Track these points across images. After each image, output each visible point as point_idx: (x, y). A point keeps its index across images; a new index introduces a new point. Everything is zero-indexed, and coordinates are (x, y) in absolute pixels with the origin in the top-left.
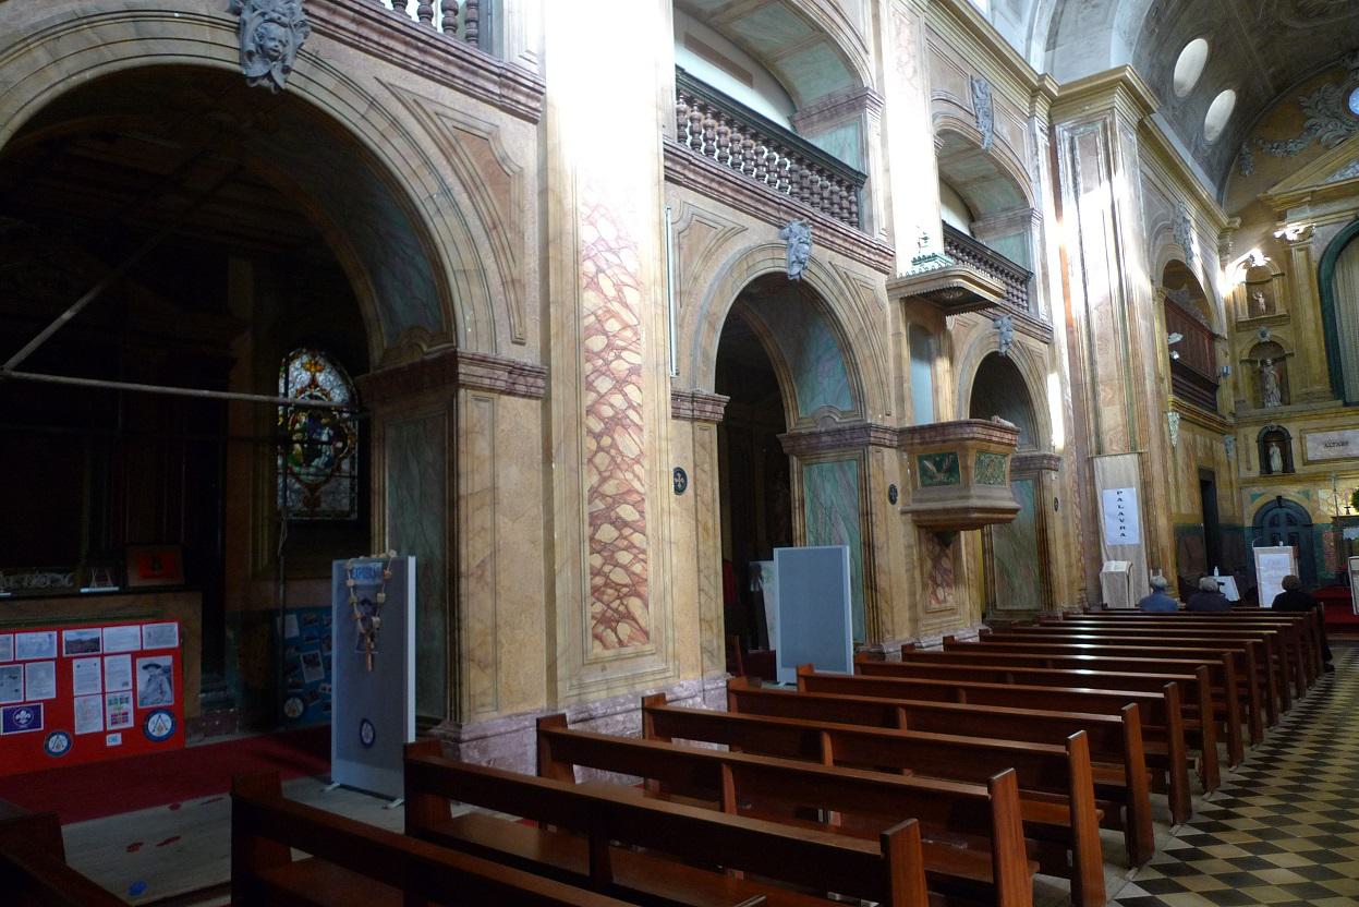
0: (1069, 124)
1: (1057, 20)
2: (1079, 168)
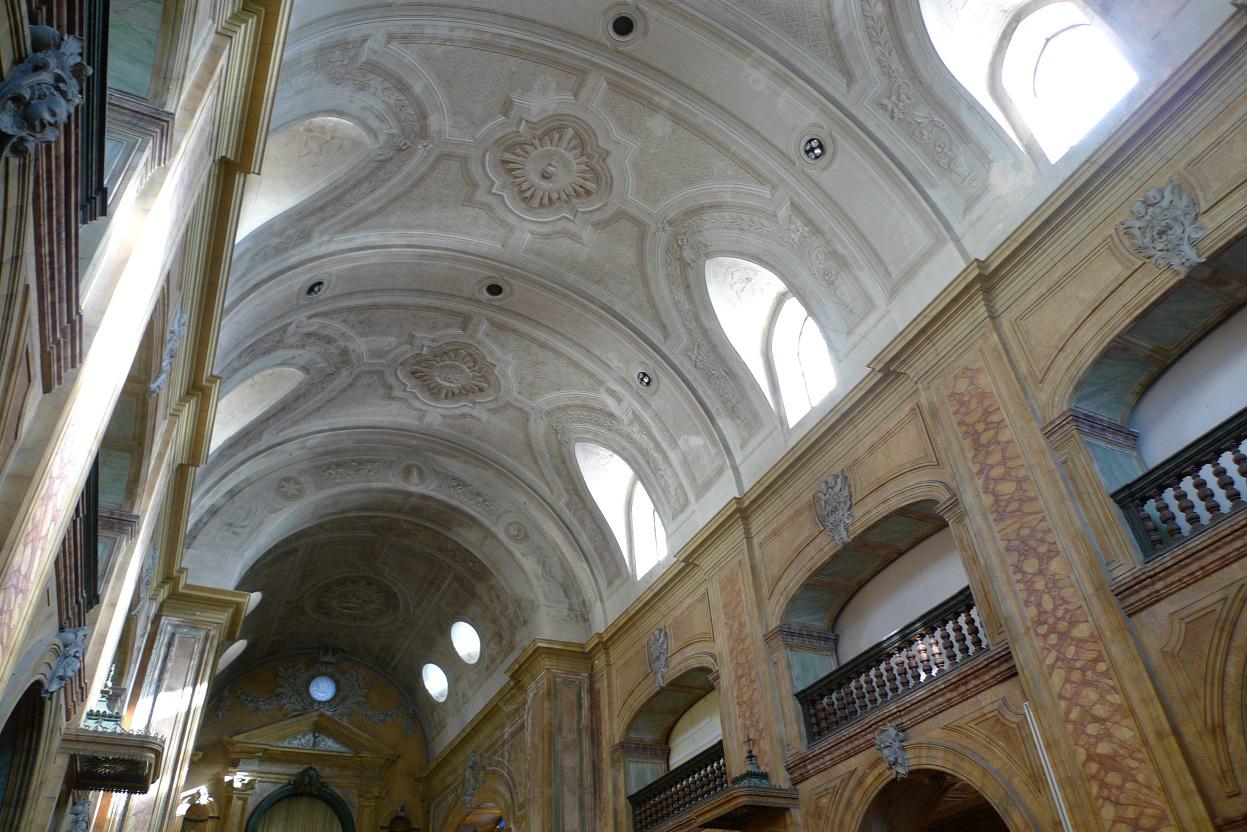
0: (175, 620)
1: (200, 526)
2: (169, 665)
